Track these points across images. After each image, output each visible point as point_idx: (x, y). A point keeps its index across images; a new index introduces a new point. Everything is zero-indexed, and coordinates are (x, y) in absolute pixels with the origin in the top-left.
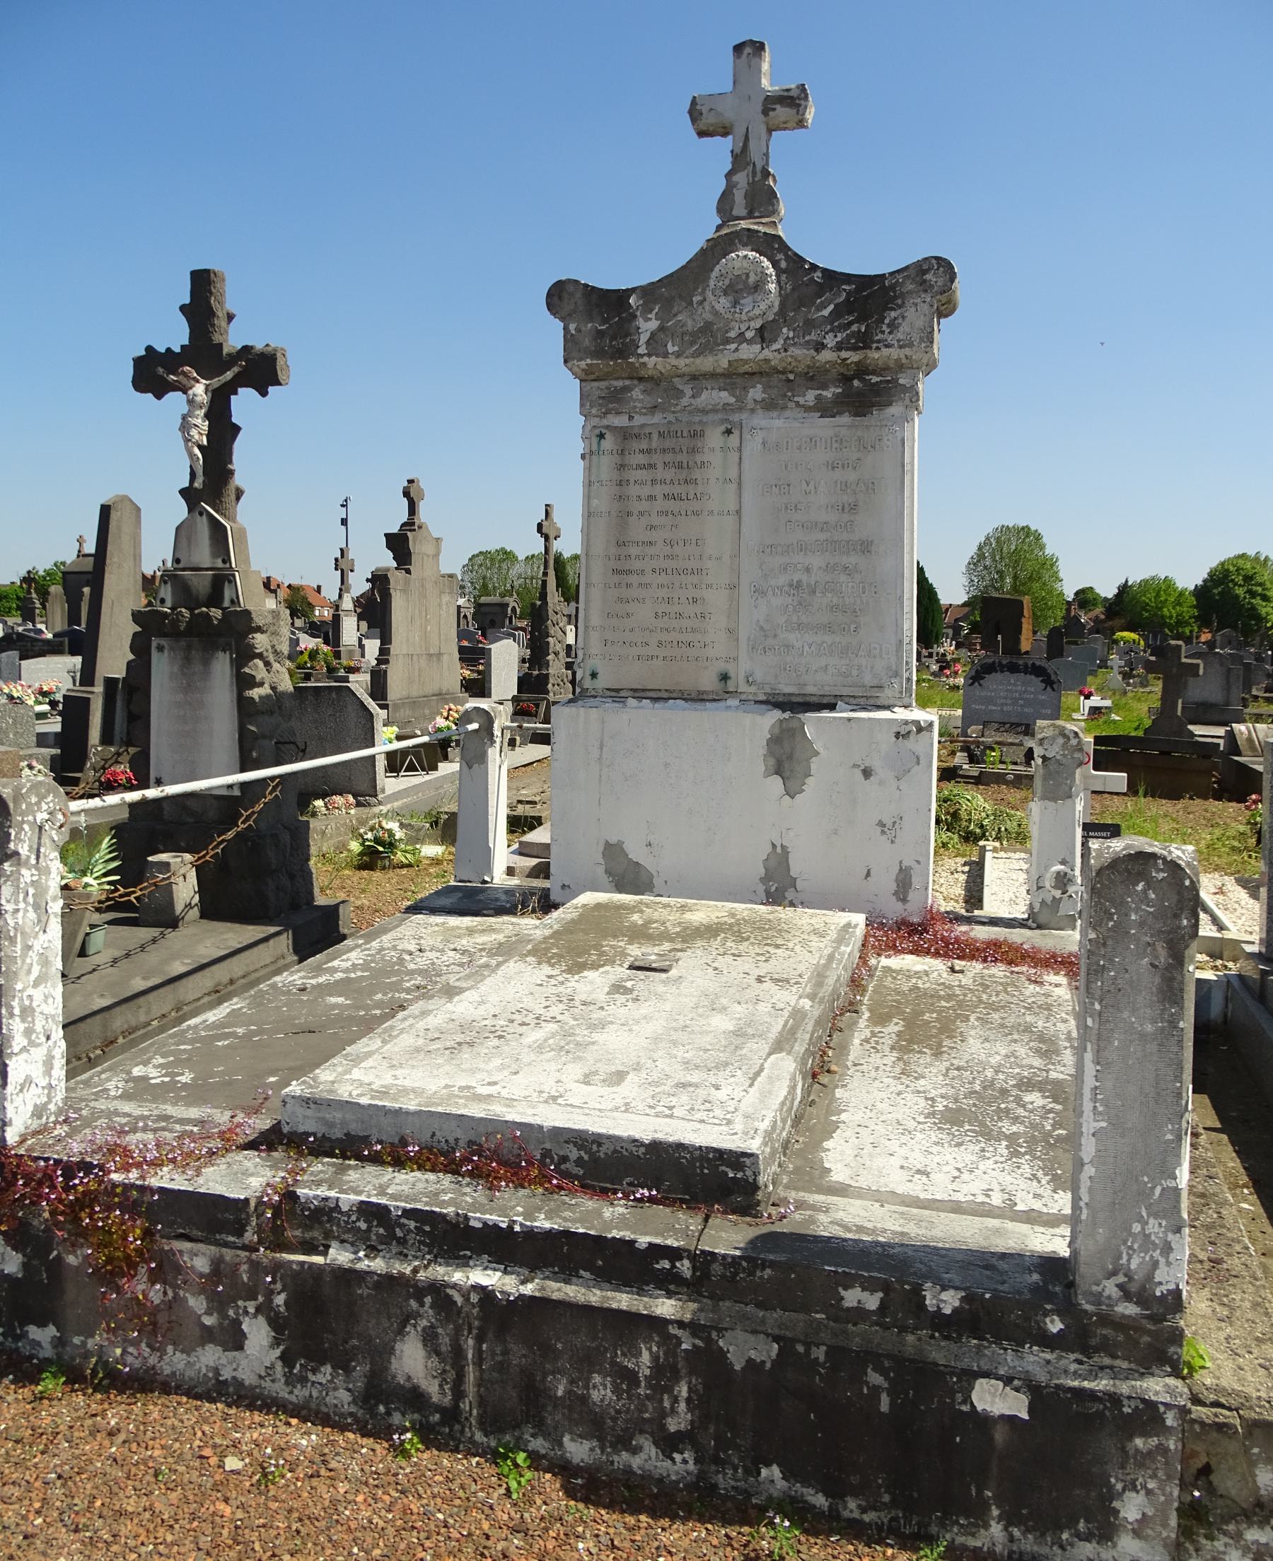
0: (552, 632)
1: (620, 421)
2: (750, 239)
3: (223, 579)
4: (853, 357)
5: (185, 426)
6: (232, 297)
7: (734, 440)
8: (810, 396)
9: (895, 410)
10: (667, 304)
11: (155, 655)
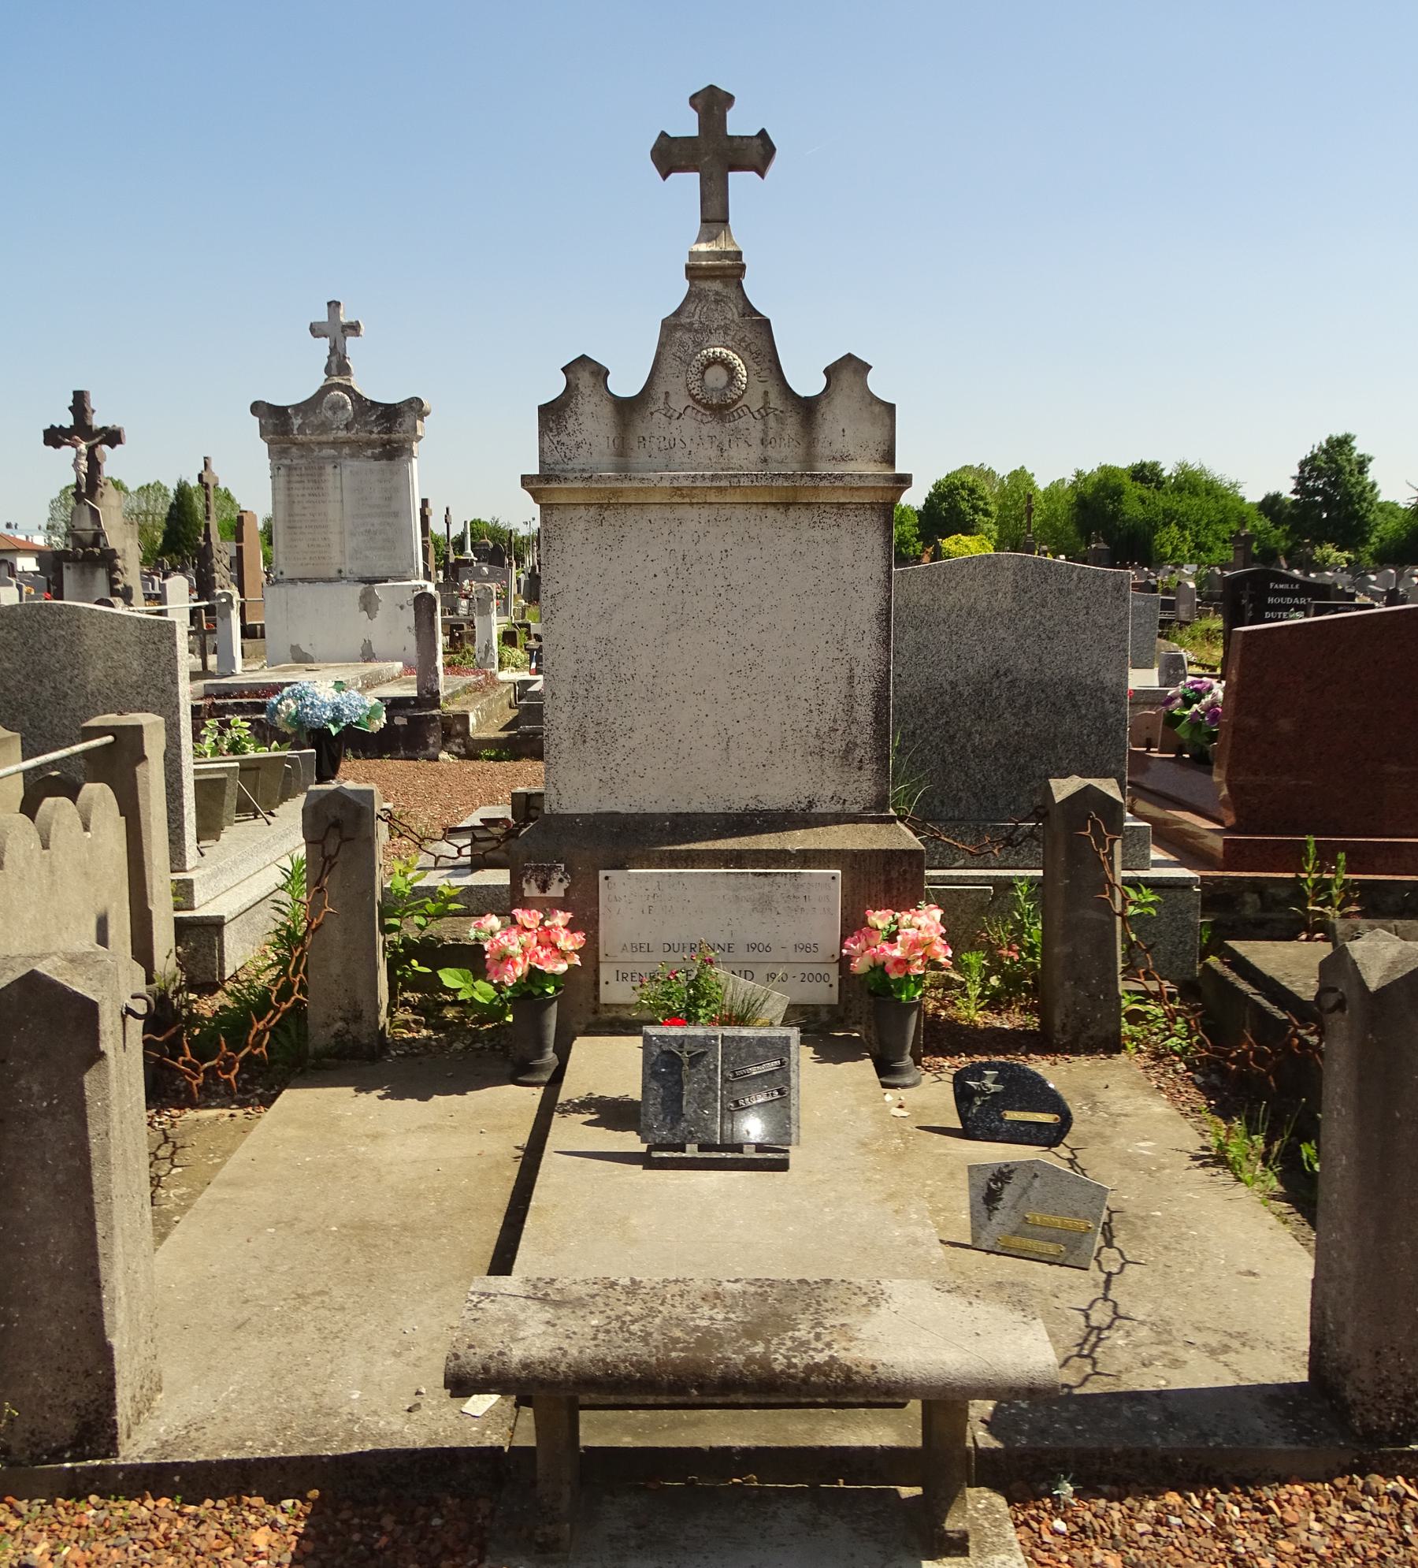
0: (217, 568)
1: (287, 462)
2: (339, 387)
3: (99, 535)
4: (385, 437)
5: (76, 465)
6: (93, 402)
7: (338, 470)
8: (369, 452)
9: (404, 457)
10: (305, 413)
11: (65, 571)
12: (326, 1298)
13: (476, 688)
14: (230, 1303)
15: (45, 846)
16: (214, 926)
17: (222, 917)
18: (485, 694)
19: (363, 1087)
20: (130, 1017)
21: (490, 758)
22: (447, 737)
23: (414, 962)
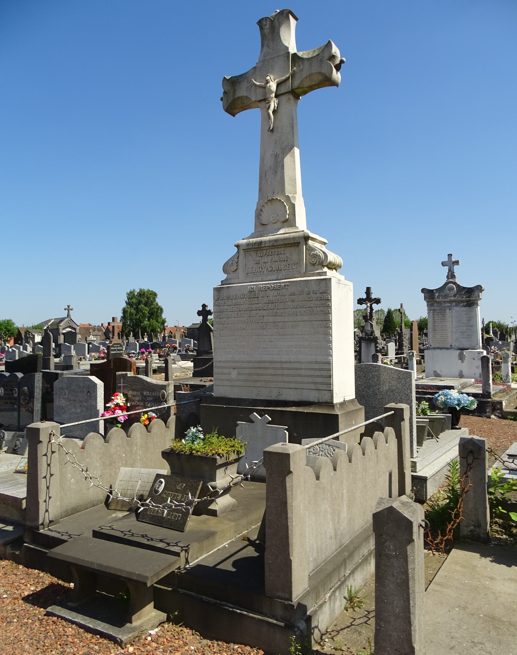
1: (433, 308)
2: (452, 282)
4: (468, 299)
6: (372, 290)
8: (462, 304)
12: (483, 646)
13: (504, 391)
14: (447, 636)
15: (376, 449)
16: (424, 480)
17: (427, 477)
18: (507, 394)
19: (484, 555)
20: (421, 527)
21: (511, 419)
22: (494, 410)
23: (500, 508)
